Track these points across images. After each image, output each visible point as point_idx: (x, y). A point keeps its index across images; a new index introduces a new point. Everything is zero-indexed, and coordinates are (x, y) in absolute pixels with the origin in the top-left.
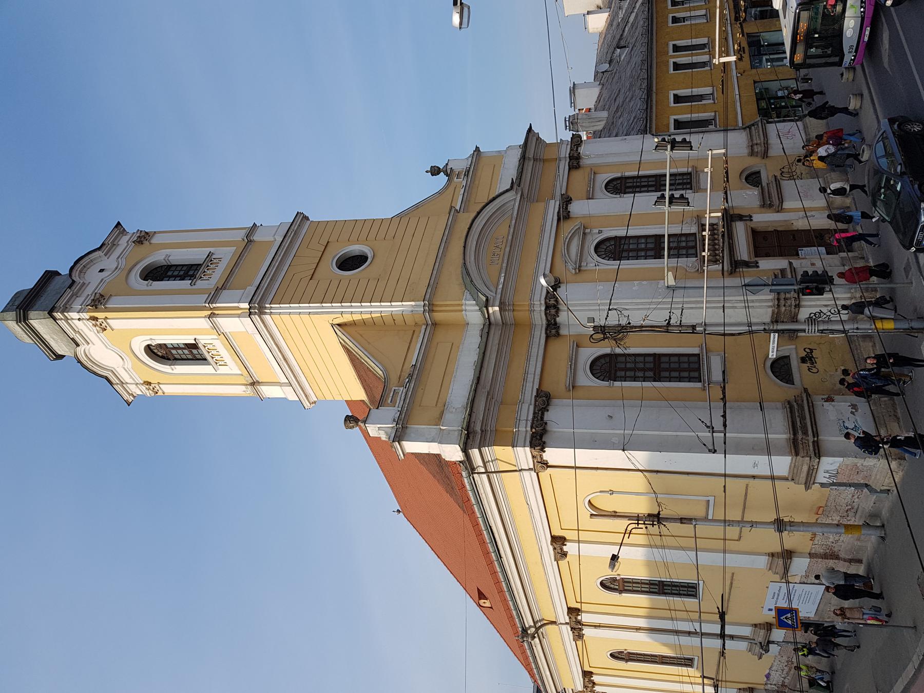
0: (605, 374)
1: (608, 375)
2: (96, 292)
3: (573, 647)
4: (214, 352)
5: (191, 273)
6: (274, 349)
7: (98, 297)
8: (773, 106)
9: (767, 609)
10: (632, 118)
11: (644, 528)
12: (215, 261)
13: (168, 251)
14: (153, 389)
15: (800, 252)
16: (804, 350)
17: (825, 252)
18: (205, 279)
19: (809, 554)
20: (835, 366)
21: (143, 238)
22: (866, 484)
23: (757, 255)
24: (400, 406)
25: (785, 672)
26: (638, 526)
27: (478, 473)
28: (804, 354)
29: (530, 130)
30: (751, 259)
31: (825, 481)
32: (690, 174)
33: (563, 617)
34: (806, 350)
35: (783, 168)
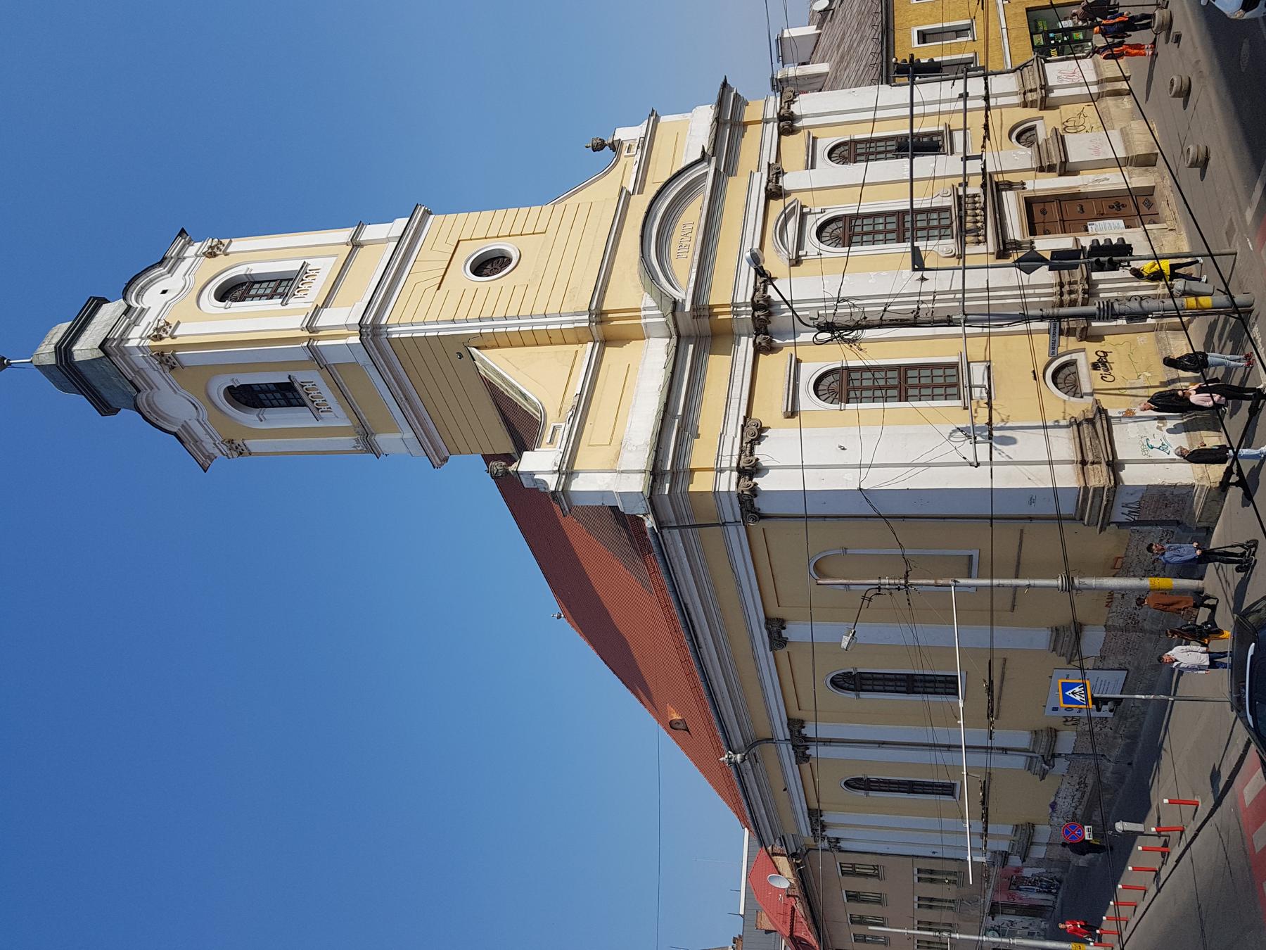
0: (834, 396)
1: (837, 397)
2: (159, 318)
3: (795, 774)
4: (313, 393)
5: (280, 290)
6: (393, 384)
7: (162, 324)
8: (1053, 42)
9: (1051, 708)
10: (862, 68)
11: (888, 595)
12: (311, 273)
13: (249, 266)
14: (237, 448)
15: (1089, 227)
16: (1096, 353)
17: (1124, 226)
19: (1105, 626)
20: (1137, 372)
22: (1178, 522)
23: (1033, 232)
24: (563, 447)
25: (1076, 800)
26: (879, 591)
27: (669, 528)
28: (1095, 359)
29: (725, 84)
30: (1024, 238)
31: (1123, 519)
32: (954, 365)
33: (782, 732)
34: (1098, 353)
35: (1067, 121)
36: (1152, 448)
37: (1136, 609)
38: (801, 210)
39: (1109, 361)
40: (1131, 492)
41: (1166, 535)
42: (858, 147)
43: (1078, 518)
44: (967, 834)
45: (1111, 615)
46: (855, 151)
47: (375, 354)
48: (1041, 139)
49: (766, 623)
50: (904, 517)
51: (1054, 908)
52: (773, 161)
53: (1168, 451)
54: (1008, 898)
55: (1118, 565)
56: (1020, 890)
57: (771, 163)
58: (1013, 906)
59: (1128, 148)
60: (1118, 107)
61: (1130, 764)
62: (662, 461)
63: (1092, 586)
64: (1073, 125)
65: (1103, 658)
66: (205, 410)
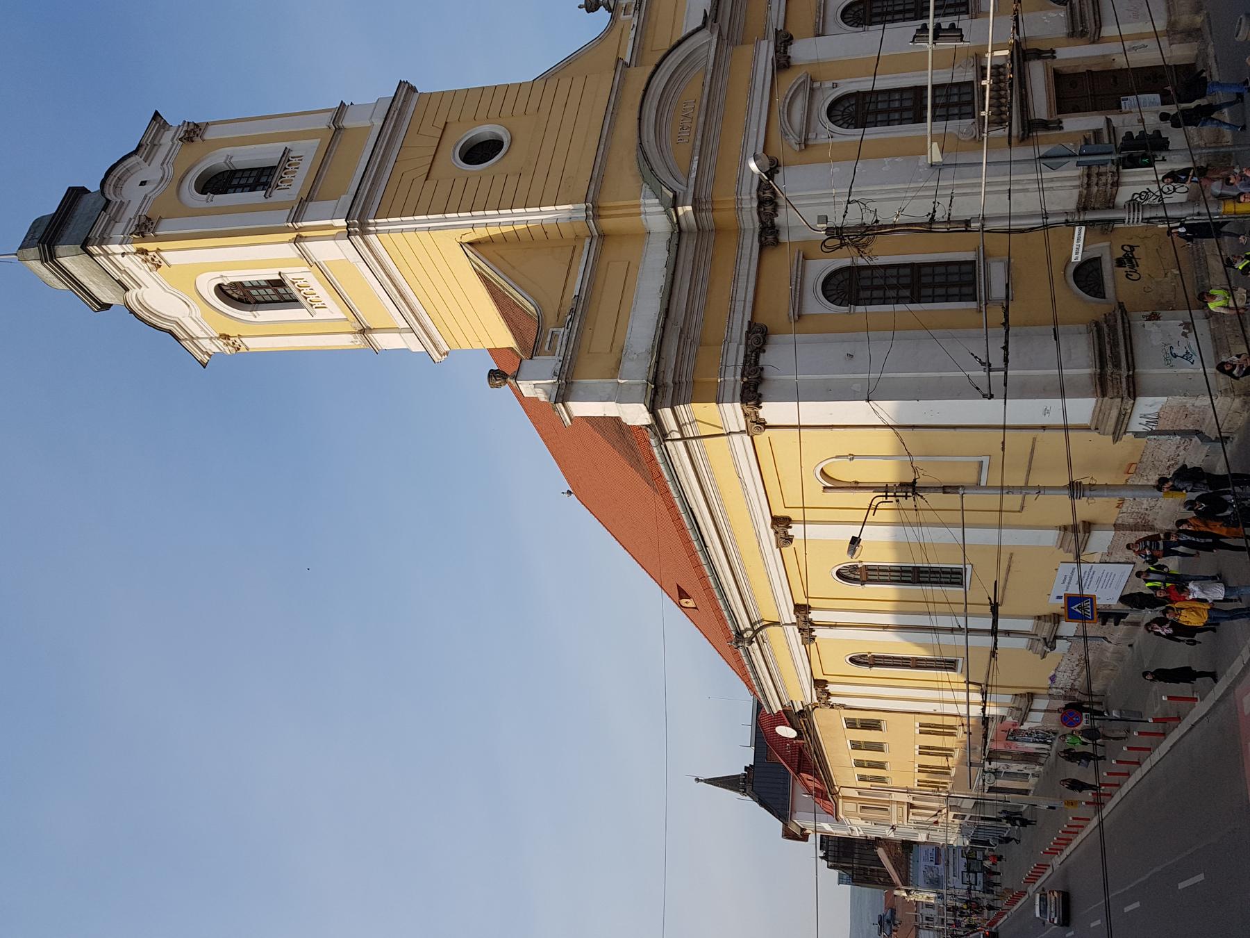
0: (843, 296)
2: (140, 214)
4: (306, 290)
5: (263, 180)
9: (1055, 597)
11: (895, 502)
14: (234, 343)
16: (1122, 247)
18: (283, 187)
20: (1164, 270)
21: (192, 133)
24: (562, 354)
25: (1075, 673)
27: (672, 440)
28: (1120, 254)
31: (1140, 429)
33: (789, 616)
34: (1125, 247)
38: (812, 84)
39: (1136, 257)
40: (1150, 404)
41: (1184, 443)
42: (874, 6)
43: (1093, 427)
44: (989, 16)
47: (365, 252)
49: (773, 524)
50: (913, 427)
51: (1049, 755)
53: (1192, 361)
54: (1005, 747)
55: (1132, 470)
56: (1017, 740)
59: (1171, 8)
61: (1131, 646)
65: (1109, 554)
66: (197, 308)
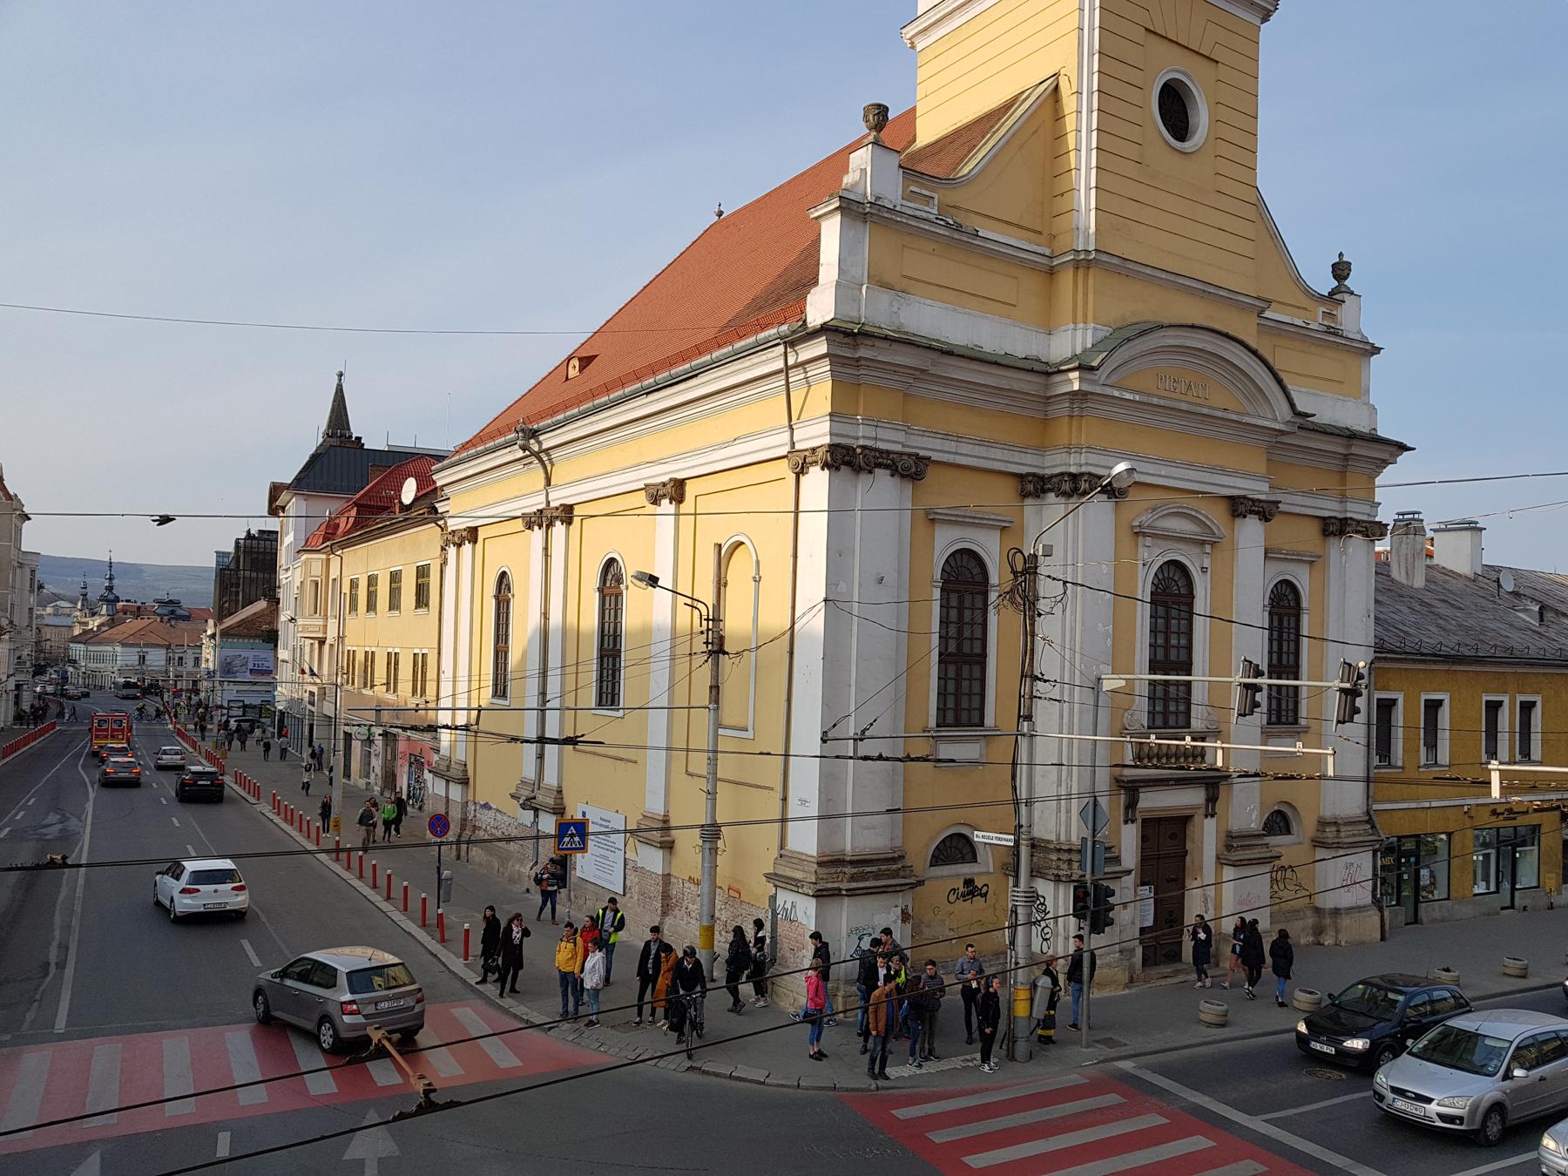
8: (1403, 860)
10: (1405, 629)
15: (1147, 887)
16: (986, 885)
17: (1145, 926)
28: (979, 883)
29: (1403, 448)
30: (1140, 812)
31: (780, 901)
32: (1296, 722)
33: (558, 497)
36: (860, 939)
37: (687, 908)
40: (808, 913)
45: (680, 880)
46: (1286, 615)
48: (1268, 840)
52: (1282, 507)
54: (401, 753)
56: (410, 766)
57: (1279, 505)
58: (394, 758)
60: (1303, 929)
62: (874, 346)
63: (843, 853)
64: (1287, 876)
65: (635, 869)
